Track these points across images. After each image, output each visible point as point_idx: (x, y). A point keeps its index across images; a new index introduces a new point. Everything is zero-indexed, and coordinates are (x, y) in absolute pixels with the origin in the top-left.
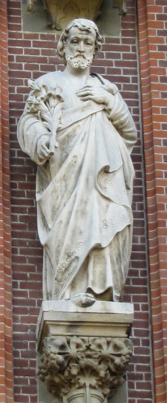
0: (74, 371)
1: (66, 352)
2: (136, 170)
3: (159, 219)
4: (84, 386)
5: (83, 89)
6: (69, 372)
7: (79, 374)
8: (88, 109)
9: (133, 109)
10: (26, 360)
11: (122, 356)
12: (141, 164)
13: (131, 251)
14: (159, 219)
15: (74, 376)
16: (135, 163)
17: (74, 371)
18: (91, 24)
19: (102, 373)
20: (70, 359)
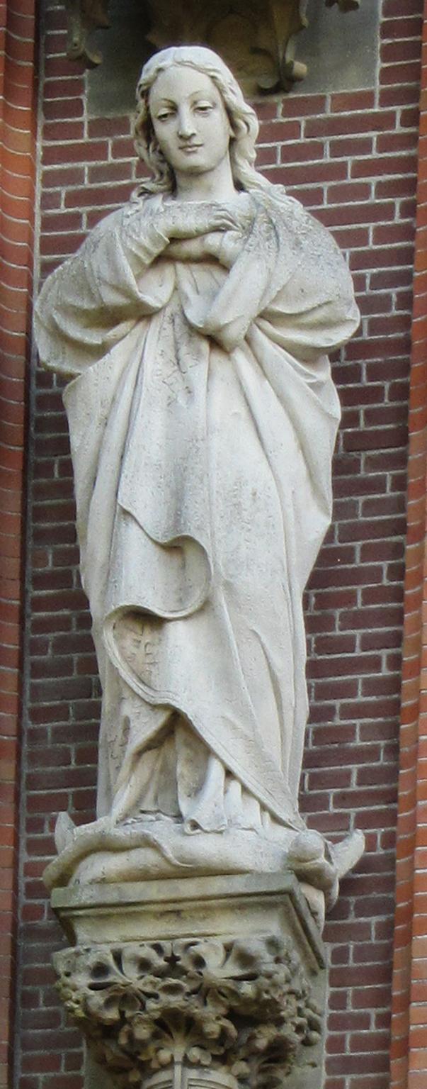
0: (143, 1032)
1: (107, 983)
2: (345, 405)
3: (420, 893)
4: (170, 1065)
5: (198, 1086)
6: (131, 1036)
7: (155, 1036)
8: (145, 546)
9: (382, 401)
10: (21, 1064)
11: (261, 977)
12: (384, 567)
13: (253, 144)
14: (420, 893)
15: (143, 1044)
16: (341, 386)
17: (143, 1032)
18: (171, 403)
19: (213, 1028)
20: (125, 998)
